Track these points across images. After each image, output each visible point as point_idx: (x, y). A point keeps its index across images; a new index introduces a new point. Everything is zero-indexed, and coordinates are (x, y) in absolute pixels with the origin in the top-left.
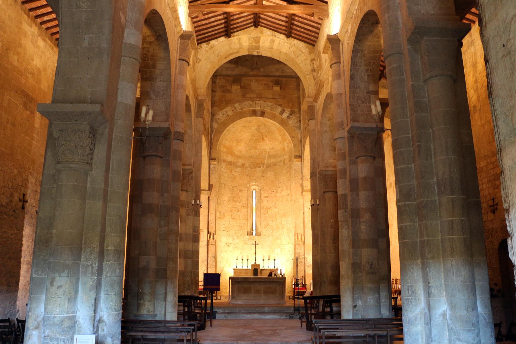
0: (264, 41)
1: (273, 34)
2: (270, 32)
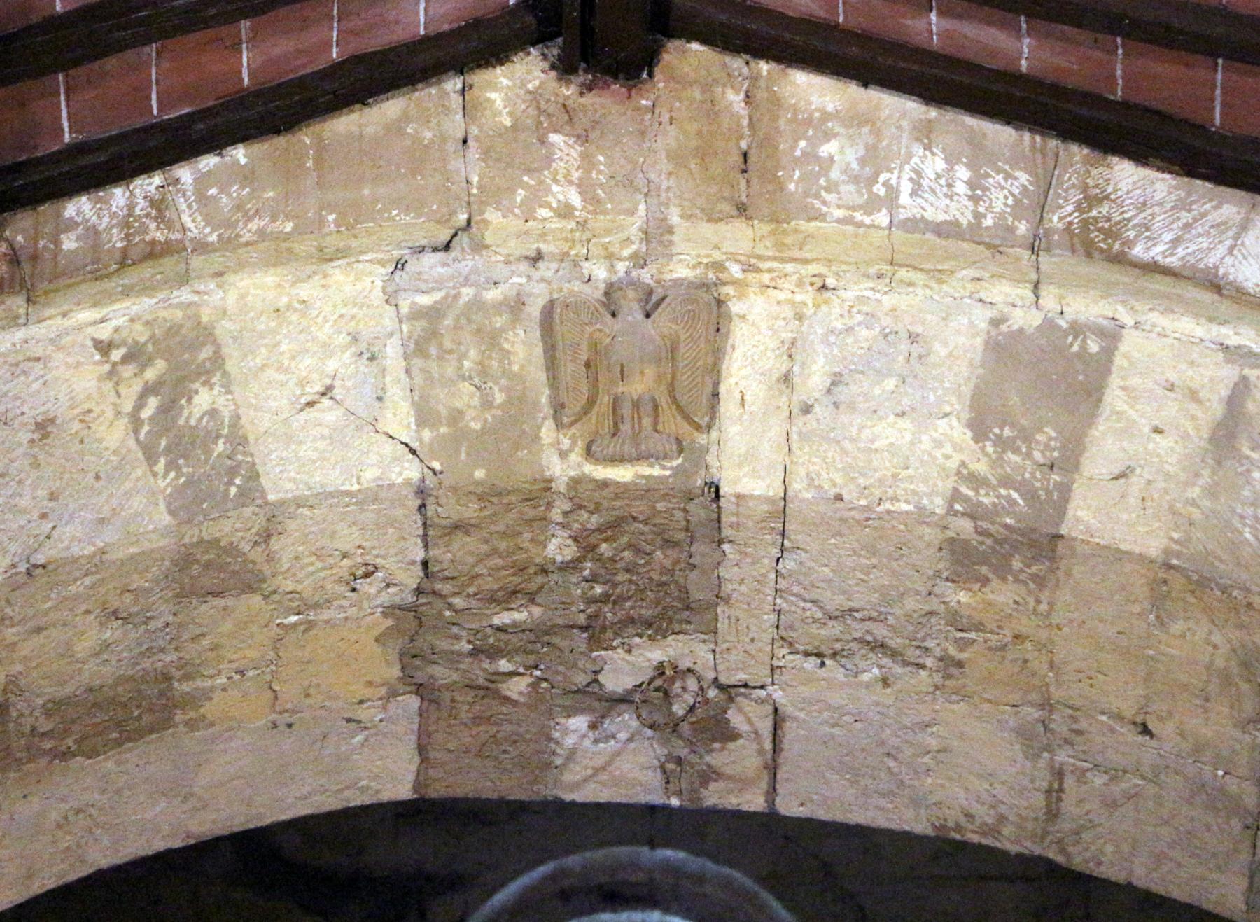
0: (814, 379)
1: (1039, 204)
2: (980, 158)
